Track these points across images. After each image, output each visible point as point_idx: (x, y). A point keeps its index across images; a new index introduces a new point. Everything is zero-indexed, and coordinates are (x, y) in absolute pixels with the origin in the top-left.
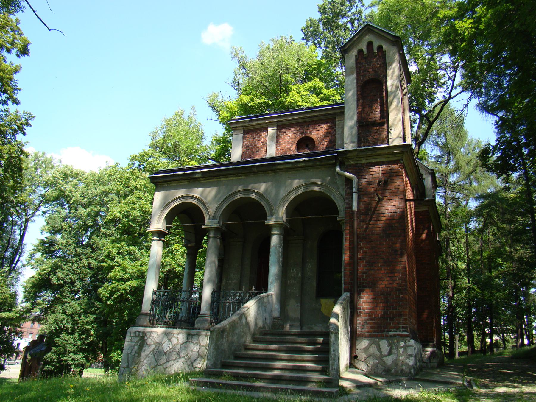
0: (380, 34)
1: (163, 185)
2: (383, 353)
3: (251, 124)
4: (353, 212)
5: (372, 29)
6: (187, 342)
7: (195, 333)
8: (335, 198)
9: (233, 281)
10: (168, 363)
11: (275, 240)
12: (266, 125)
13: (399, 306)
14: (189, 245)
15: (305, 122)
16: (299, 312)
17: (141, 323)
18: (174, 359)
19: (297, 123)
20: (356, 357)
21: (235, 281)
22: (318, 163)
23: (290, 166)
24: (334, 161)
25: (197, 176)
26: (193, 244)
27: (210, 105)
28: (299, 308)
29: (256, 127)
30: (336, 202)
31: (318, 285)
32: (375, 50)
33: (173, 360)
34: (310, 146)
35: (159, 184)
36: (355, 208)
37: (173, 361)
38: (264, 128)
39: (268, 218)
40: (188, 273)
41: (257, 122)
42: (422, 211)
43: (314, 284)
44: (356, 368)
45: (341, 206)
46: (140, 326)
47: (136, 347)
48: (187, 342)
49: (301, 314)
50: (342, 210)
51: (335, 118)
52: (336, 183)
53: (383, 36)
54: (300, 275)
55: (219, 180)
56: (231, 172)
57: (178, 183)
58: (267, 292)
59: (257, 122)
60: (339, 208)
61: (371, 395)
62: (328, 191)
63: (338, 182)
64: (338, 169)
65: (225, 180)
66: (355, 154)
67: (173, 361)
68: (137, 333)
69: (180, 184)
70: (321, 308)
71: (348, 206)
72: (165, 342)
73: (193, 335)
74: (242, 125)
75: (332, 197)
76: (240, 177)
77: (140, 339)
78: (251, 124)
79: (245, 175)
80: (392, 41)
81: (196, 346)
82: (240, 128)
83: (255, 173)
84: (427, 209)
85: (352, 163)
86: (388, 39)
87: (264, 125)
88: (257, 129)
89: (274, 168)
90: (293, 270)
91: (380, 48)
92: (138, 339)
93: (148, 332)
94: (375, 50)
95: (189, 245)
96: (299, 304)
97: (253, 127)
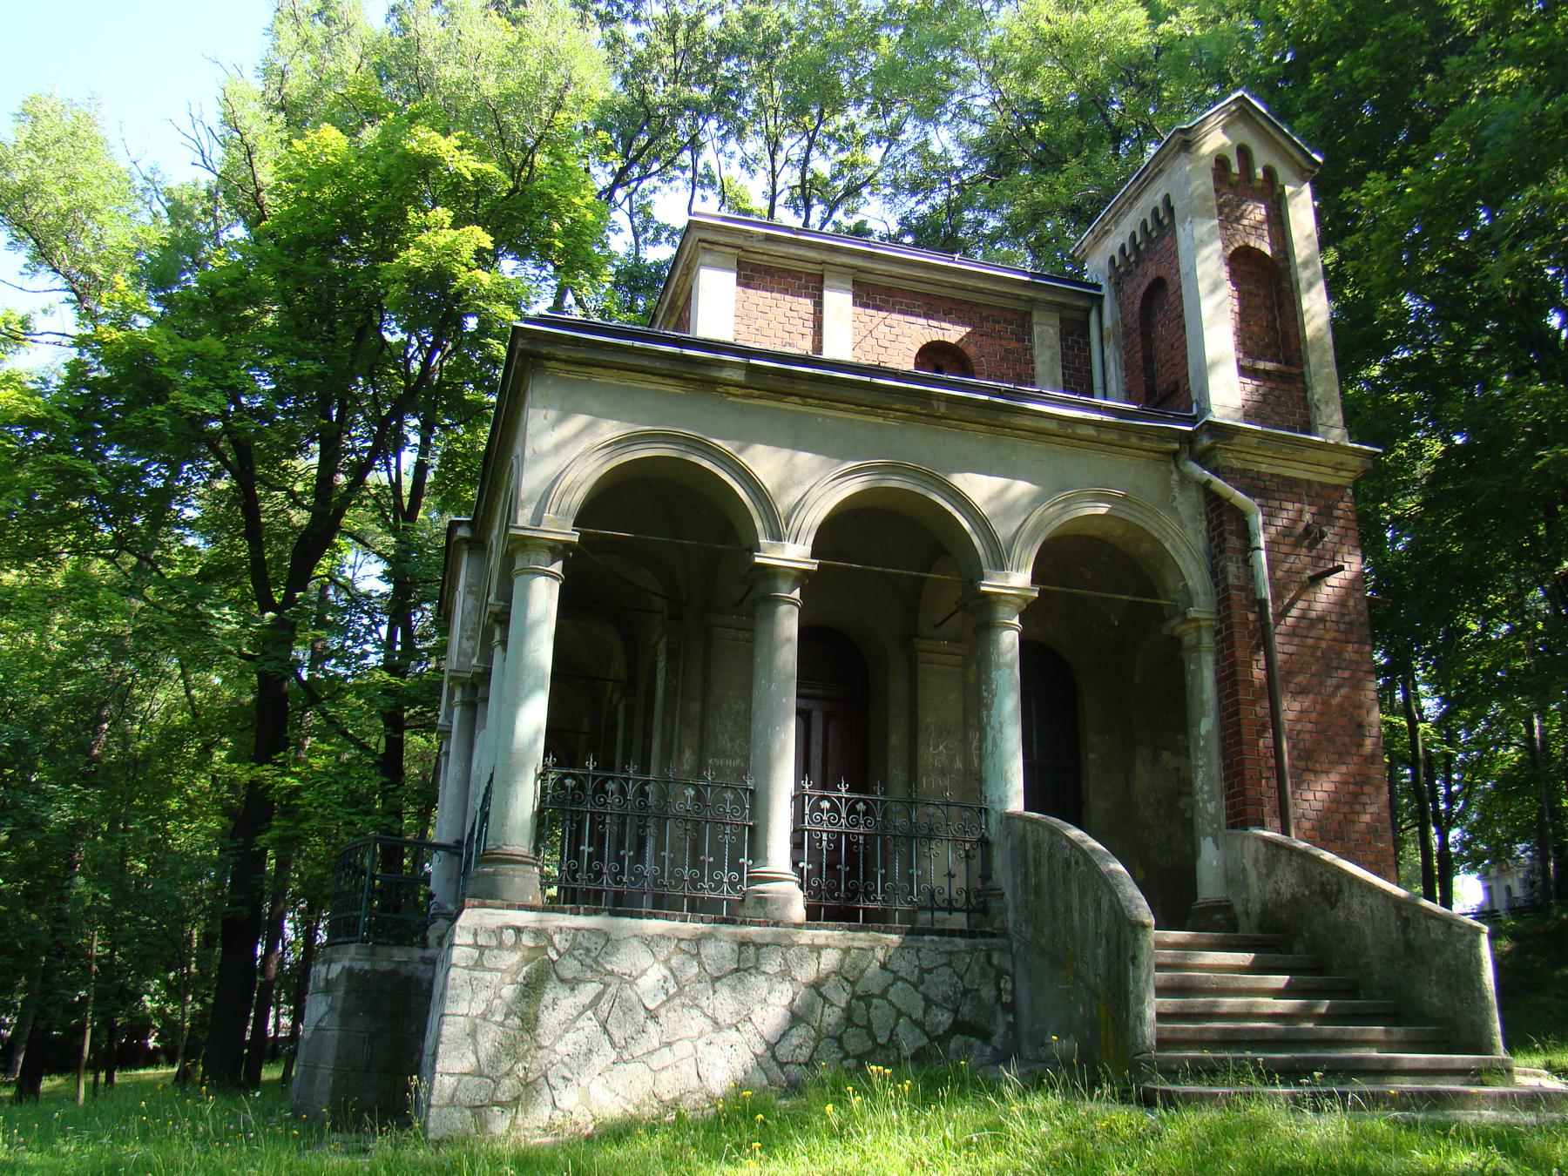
0: (1272, 137)
1: (568, 372)
5: (1251, 112)
7: (768, 940)
8: (1177, 552)
9: (729, 762)
12: (821, 268)
15: (940, 297)
17: (511, 894)
18: (696, 1033)
22: (1134, 440)
23: (1051, 426)
24: (1176, 446)
25: (727, 374)
30: (1180, 564)
33: (688, 1038)
35: (554, 364)
37: (687, 1042)
38: (808, 274)
41: (792, 250)
46: (510, 907)
52: (1175, 509)
53: (1279, 144)
55: (803, 409)
57: (634, 380)
58: (255, 789)
59: (792, 250)
61: (607, 1116)
62: (1157, 526)
63: (1180, 509)
65: (824, 416)
67: (687, 1042)
68: (509, 937)
69: (645, 386)
72: (644, 972)
74: (739, 242)
75: (1167, 545)
76: (880, 420)
79: (899, 418)
80: (1300, 165)
81: (778, 987)
82: (728, 250)
83: (933, 418)
86: (1291, 156)
87: (809, 265)
89: (1004, 418)
90: (936, 747)
91: (1269, 172)
94: (1259, 173)
97: (772, 259)
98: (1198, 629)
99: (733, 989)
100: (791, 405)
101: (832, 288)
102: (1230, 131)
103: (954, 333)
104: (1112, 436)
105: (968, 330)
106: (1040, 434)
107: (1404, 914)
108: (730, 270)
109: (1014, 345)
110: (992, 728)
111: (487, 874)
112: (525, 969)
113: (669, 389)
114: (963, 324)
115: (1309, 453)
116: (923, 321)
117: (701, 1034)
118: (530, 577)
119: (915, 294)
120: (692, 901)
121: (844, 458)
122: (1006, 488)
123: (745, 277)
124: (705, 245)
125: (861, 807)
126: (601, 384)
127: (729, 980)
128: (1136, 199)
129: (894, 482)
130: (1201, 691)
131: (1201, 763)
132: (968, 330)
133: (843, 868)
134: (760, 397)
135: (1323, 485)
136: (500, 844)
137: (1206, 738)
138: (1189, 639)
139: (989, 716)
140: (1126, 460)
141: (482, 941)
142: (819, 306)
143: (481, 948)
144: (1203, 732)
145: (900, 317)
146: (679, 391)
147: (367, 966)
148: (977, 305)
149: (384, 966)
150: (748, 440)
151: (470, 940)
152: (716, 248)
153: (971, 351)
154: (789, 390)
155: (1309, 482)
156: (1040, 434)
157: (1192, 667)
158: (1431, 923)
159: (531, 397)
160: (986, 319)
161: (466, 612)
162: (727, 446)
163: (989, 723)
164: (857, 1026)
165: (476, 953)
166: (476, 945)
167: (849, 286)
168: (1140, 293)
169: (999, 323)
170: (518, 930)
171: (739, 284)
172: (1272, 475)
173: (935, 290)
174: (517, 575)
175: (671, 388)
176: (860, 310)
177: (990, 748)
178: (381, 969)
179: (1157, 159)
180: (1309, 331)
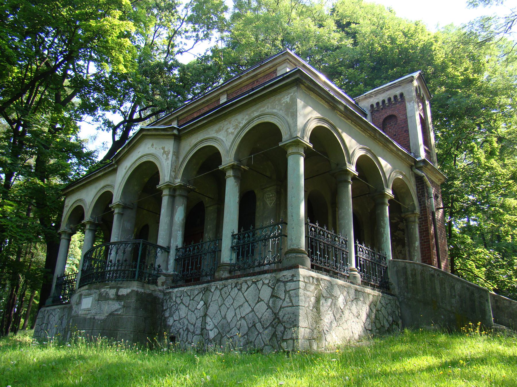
1: (305, 90)
55: (351, 124)
98: (415, 217)
107: (496, 298)
110: (385, 234)
111: (300, 257)
112: (316, 292)
113: (326, 106)
118: (300, 156)
121: (360, 144)
124: (288, 61)
126: (312, 98)
128: (387, 91)
130: (416, 234)
131: (416, 254)
134: (343, 117)
136: (299, 247)
137: (417, 247)
138: (412, 219)
139: (384, 231)
144: (416, 246)
147: (143, 291)
149: (148, 291)
150: (343, 131)
152: (291, 63)
154: (350, 118)
156: (391, 151)
157: (413, 227)
158: (505, 301)
161: (173, 162)
162: (340, 131)
163: (384, 232)
164: (197, 335)
168: (385, 116)
170: (313, 278)
174: (289, 156)
177: (385, 240)
178: (147, 293)
179: (401, 82)
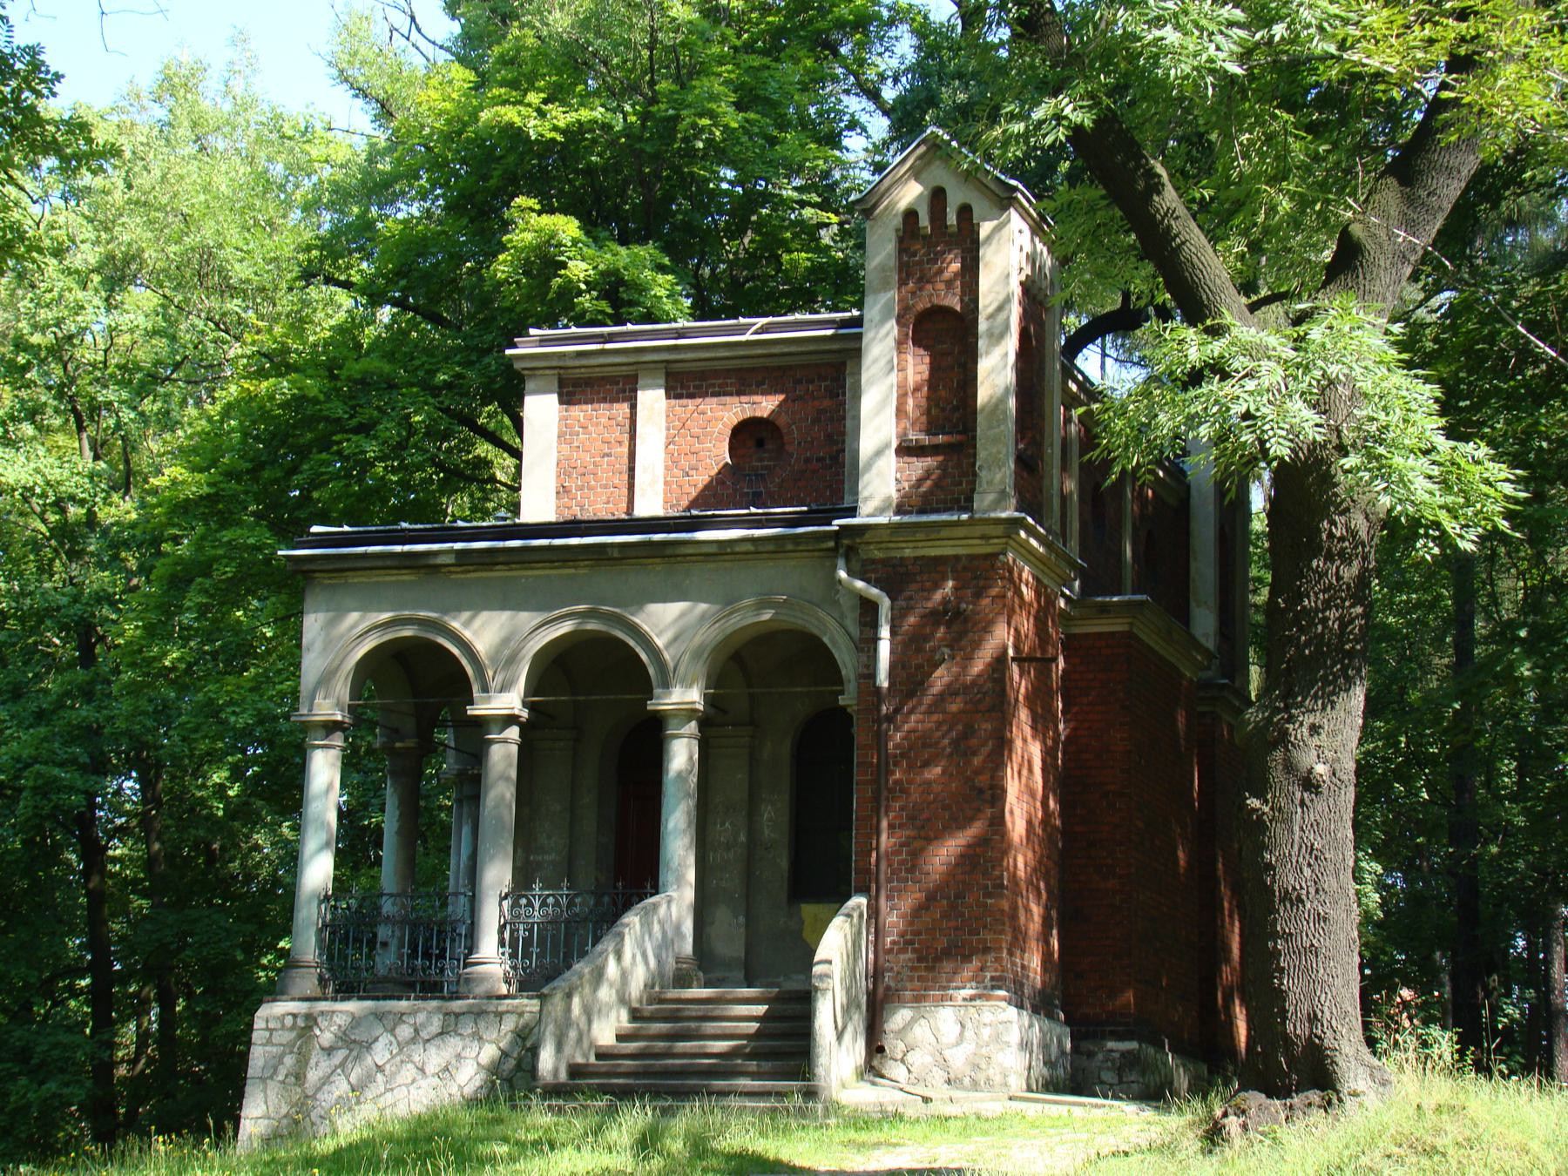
2: (944, 1040)
3: (584, 362)
4: (878, 690)
6: (441, 1034)
9: (546, 857)
10: (389, 1095)
11: (681, 755)
13: (985, 927)
14: (398, 745)
16: (743, 942)
19: (728, 370)
20: (881, 1050)
21: (552, 857)
22: (790, 547)
25: (440, 560)
26: (411, 743)
27: (344, 78)
28: (742, 930)
29: (598, 372)
30: (836, 655)
31: (795, 864)
32: (952, 219)
34: (769, 446)
36: (883, 680)
39: (657, 691)
40: (399, 832)
42: (1113, 634)
43: (784, 863)
44: (883, 1077)
45: (849, 665)
47: (289, 1061)
48: (441, 1034)
49: (749, 948)
50: (852, 677)
51: (844, 364)
52: (836, 603)
54: (743, 838)
56: (547, 556)
60: (844, 672)
64: (843, 574)
65: (527, 577)
66: (885, 535)
69: (387, 579)
70: (801, 930)
71: (866, 671)
73: (457, 1015)
74: (554, 364)
75: (826, 640)
76: (572, 571)
77: (300, 1037)
78: (584, 362)
84: (1126, 628)
85: (878, 555)
88: (603, 378)
89: (669, 551)
90: (723, 824)
92: (293, 1035)
93: (322, 1013)
94: (952, 219)
95: (398, 745)
96: (742, 919)
99: (438, 1047)
100: (499, 573)
101: (647, 387)
102: (924, 176)
103: (766, 405)
104: (771, 547)
105: (781, 397)
106: (708, 556)
108: (550, 392)
109: (827, 403)
114: (776, 392)
115: (945, 533)
116: (735, 399)
117: (414, 1081)
119: (727, 373)
120: (423, 983)
122: (690, 610)
123: (569, 394)
125: (551, 900)
127: (437, 1041)
129: (592, 625)
132: (781, 397)
133: (535, 950)
135: (971, 557)
140: (793, 563)
141: (271, 1025)
142: (633, 407)
143: (271, 1031)
145: (715, 400)
146: (412, 578)
148: (790, 368)
151: (263, 1025)
153: (782, 421)
155: (957, 558)
159: (309, 603)
160: (799, 382)
165: (267, 1034)
166: (267, 1029)
167: (662, 381)
169: (812, 382)
170: (295, 1016)
171: (561, 402)
172: (916, 558)
173: (746, 363)
175: (407, 577)
176: (673, 401)
180: (984, 394)
